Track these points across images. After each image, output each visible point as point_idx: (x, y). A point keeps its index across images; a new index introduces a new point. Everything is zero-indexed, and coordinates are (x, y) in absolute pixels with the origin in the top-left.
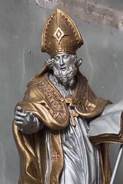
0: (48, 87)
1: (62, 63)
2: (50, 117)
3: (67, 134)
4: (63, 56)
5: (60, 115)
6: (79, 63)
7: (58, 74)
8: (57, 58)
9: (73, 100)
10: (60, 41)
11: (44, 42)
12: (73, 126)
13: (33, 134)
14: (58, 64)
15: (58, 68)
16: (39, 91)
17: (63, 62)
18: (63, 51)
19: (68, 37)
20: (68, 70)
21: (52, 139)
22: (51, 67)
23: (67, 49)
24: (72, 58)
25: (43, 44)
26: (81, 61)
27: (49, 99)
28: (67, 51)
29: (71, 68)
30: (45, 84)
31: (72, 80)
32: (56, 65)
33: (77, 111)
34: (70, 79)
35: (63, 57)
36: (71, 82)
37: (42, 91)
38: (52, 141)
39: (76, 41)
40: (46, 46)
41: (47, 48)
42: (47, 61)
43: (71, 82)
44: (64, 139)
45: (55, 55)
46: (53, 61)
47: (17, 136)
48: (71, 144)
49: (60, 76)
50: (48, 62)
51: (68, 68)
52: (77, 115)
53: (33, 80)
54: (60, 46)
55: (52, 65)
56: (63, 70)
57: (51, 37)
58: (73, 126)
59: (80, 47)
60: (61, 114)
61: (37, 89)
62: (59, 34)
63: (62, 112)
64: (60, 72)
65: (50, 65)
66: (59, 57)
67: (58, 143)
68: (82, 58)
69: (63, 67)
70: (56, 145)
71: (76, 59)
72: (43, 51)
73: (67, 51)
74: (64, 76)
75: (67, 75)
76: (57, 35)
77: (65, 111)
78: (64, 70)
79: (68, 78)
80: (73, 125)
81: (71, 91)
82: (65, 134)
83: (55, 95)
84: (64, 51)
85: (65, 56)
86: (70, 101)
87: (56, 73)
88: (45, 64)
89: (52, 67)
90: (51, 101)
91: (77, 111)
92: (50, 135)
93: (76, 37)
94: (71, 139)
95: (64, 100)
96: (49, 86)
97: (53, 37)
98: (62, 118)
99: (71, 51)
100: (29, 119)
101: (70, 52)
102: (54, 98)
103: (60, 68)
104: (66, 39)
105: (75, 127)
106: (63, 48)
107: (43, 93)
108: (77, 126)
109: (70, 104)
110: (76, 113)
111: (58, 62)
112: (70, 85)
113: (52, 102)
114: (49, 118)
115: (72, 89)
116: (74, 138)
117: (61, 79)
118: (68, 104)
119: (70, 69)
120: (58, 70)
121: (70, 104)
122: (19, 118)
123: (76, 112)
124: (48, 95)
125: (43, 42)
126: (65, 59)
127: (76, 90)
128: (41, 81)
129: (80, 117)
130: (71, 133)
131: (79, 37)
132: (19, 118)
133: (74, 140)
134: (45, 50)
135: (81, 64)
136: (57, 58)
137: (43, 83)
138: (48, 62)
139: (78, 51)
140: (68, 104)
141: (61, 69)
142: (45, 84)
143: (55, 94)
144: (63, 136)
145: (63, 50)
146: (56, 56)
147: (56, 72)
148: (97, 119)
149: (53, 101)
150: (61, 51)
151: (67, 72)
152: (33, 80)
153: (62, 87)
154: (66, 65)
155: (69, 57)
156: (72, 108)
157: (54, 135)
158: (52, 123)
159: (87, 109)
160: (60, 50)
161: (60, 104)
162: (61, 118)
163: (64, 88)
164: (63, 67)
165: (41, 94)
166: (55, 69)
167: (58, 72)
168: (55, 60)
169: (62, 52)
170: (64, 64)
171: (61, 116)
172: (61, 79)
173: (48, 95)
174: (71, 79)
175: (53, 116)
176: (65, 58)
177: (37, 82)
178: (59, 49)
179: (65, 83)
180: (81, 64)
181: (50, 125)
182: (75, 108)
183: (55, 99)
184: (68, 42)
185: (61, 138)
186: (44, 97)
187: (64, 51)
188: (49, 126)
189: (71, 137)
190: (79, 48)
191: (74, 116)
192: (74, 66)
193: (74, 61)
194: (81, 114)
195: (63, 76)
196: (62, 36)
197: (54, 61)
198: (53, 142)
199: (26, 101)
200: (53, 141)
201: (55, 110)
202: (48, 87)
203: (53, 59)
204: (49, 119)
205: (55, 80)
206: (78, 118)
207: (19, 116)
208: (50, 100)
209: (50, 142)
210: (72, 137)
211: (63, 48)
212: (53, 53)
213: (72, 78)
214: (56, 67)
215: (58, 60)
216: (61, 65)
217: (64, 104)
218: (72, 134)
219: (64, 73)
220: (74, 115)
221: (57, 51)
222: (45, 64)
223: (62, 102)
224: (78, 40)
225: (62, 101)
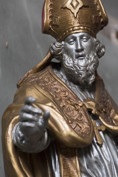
0: (55, 85)
1: (79, 48)
2: (66, 126)
3: (89, 157)
4: (81, 37)
5: (79, 126)
6: (101, 51)
7: (71, 65)
8: (71, 40)
9: (97, 105)
10: (77, 13)
11: (49, 16)
12: (98, 144)
13: (30, 154)
14: (72, 50)
15: (71, 56)
16: (41, 91)
17: (81, 45)
18: (81, 29)
19: (89, 9)
20: (88, 59)
21: (64, 165)
22: (59, 55)
23: (88, 27)
24: (94, 41)
25: (47, 19)
26: (103, 50)
27: (59, 102)
28: (88, 30)
29: (92, 57)
30: (49, 81)
31: (93, 76)
32: (68, 51)
33: (104, 123)
34: (90, 73)
35: (79, 38)
36: (92, 79)
37: (46, 89)
38: (64, 168)
39: (98, 16)
40: (51, 22)
41: (53, 25)
42: (54, 46)
43: (92, 79)
44: (85, 165)
45: (68, 36)
46: (63, 45)
47: (11, 156)
48: (96, 173)
49: (75, 67)
50: (56, 47)
51: (89, 56)
52: (103, 129)
53: (28, 75)
54: (76, 22)
55: (62, 52)
56: (80, 59)
57: (62, 8)
58: (98, 144)
59: (102, 28)
60: (80, 125)
61: (37, 87)
62: (75, 4)
63: (82, 122)
64: (76, 62)
65: (59, 51)
66: (75, 39)
67: (76, 171)
68: (105, 46)
69: (80, 54)
70: (71, 173)
71: (98, 45)
72: (46, 31)
73: (88, 30)
74: (82, 68)
75: (87, 66)
76: (71, 4)
77: (86, 121)
78: (82, 59)
79: (87, 71)
80: (98, 142)
81: (88, 94)
82: (86, 157)
83: (67, 96)
84: (84, 29)
85: (84, 37)
86: (92, 106)
87: (69, 64)
88: (50, 50)
89: (61, 55)
90: (61, 106)
91: (104, 123)
92: (61, 159)
93: (99, 11)
94: (95, 166)
95: (84, 105)
96: (56, 83)
97: (66, 8)
98: (83, 130)
99: (92, 31)
100: (41, 122)
101: (91, 32)
102: (66, 102)
103: (75, 56)
104: (85, 11)
105: (101, 146)
106: (82, 25)
107: (49, 92)
108: (104, 146)
109: (92, 110)
110: (101, 125)
111: (73, 47)
112: (90, 83)
113: (63, 107)
114: (64, 127)
115: (90, 92)
116: (99, 164)
117: (76, 73)
118: (90, 111)
119: (91, 58)
120: (71, 59)
121: (92, 110)
122: (30, 116)
123: (101, 124)
124: (56, 96)
125: (47, 17)
126: (85, 42)
127: (96, 93)
128: (44, 76)
129: (107, 132)
130: (95, 156)
131: (103, 12)
132: (30, 116)
133: (99, 166)
134: (50, 29)
135: (104, 53)
136: (71, 40)
137: (46, 80)
138: (56, 47)
139: (99, 35)
140: (90, 111)
141: (78, 57)
142: (49, 81)
143: (67, 95)
144: (83, 161)
145: (81, 28)
146: (70, 37)
147: (69, 62)
148: (113, 155)
149: (64, 106)
150: (78, 30)
151: (87, 62)
152: (28, 75)
153: (75, 87)
154: (85, 51)
155: (89, 40)
156: (95, 117)
157: (67, 157)
158: (70, 136)
159: (114, 122)
160: (76, 28)
161: (77, 110)
162: (81, 131)
163: (77, 89)
164: (80, 54)
165: (45, 93)
166: (66, 57)
167: (72, 62)
168: (67, 43)
169: (81, 31)
170: (82, 50)
171: (80, 127)
172: (76, 73)
173: (56, 96)
174: (92, 73)
175: (70, 127)
176: (85, 40)
177: (35, 78)
178: (70, 27)
179: (83, 78)
180: (104, 53)
181: (67, 140)
182: (100, 117)
183: (68, 103)
184: (89, 17)
185: (80, 163)
186: (50, 97)
187: (84, 29)
188: (65, 141)
189: (96, 162)
190: (100, 31)
191: (100, 130)
192: (95, 54)
193: (96, 46)
194: (111, 127)
195: (80, 68)
196: (79, 7)
197: (65, 45)
198: (67, 168)
199: (20, 101)
200: (67, 168)
201: (69, 118)
202: (55, 85)
203: (63, 43)
204: (65, 129)
205: (62, 76)
206: (104, 133)
207: (29, 112)
208: (60, 104)
209: (60, 168)
210: (97, 161)
211: (82, 25)
212: (65, 31)
213: (93, 72)
214: (68, 55)
215: (72, 43)
216: (77, 51)
217: (84, 110)
218: (96, 158)
219: (82, 63)
220: (99, 129)
221: (71, 29)
222: (50, 50)
223: (81, 106)
224: (101, 17)
225: (80, 105)
